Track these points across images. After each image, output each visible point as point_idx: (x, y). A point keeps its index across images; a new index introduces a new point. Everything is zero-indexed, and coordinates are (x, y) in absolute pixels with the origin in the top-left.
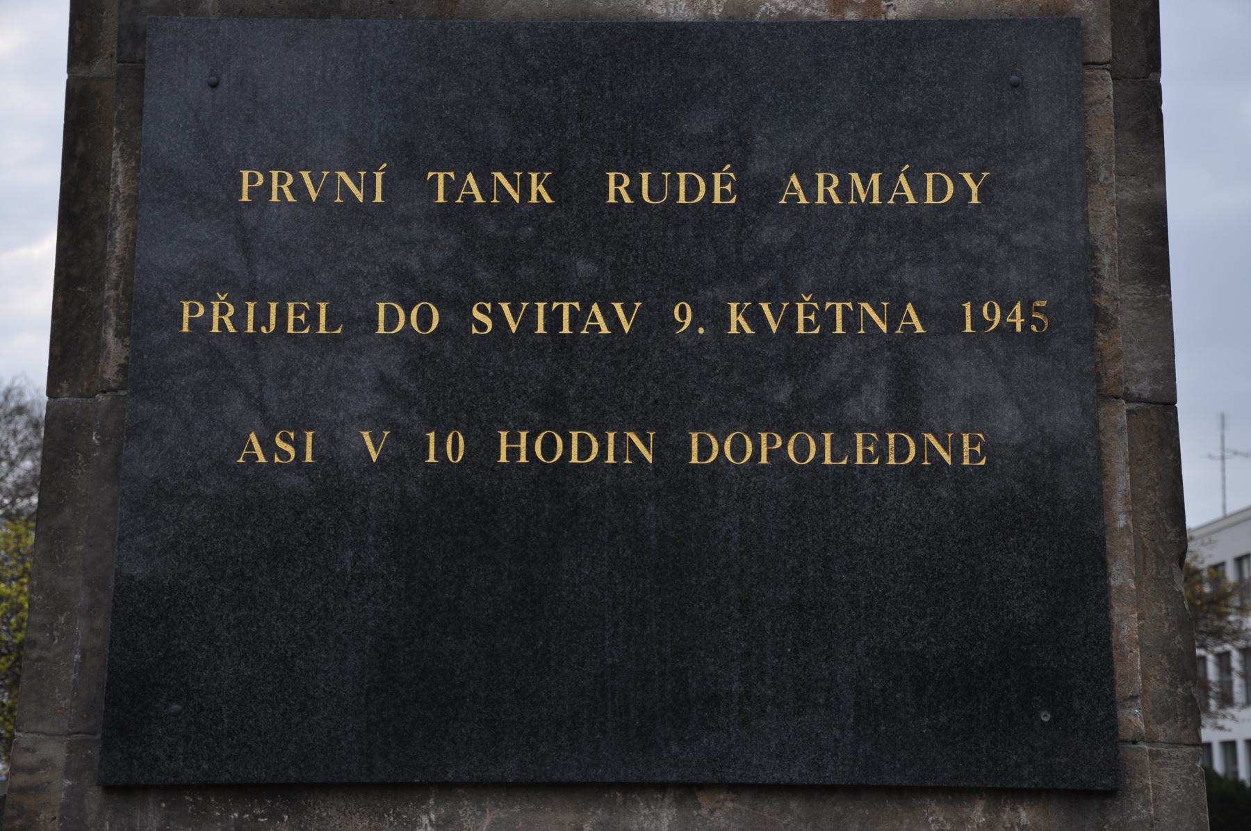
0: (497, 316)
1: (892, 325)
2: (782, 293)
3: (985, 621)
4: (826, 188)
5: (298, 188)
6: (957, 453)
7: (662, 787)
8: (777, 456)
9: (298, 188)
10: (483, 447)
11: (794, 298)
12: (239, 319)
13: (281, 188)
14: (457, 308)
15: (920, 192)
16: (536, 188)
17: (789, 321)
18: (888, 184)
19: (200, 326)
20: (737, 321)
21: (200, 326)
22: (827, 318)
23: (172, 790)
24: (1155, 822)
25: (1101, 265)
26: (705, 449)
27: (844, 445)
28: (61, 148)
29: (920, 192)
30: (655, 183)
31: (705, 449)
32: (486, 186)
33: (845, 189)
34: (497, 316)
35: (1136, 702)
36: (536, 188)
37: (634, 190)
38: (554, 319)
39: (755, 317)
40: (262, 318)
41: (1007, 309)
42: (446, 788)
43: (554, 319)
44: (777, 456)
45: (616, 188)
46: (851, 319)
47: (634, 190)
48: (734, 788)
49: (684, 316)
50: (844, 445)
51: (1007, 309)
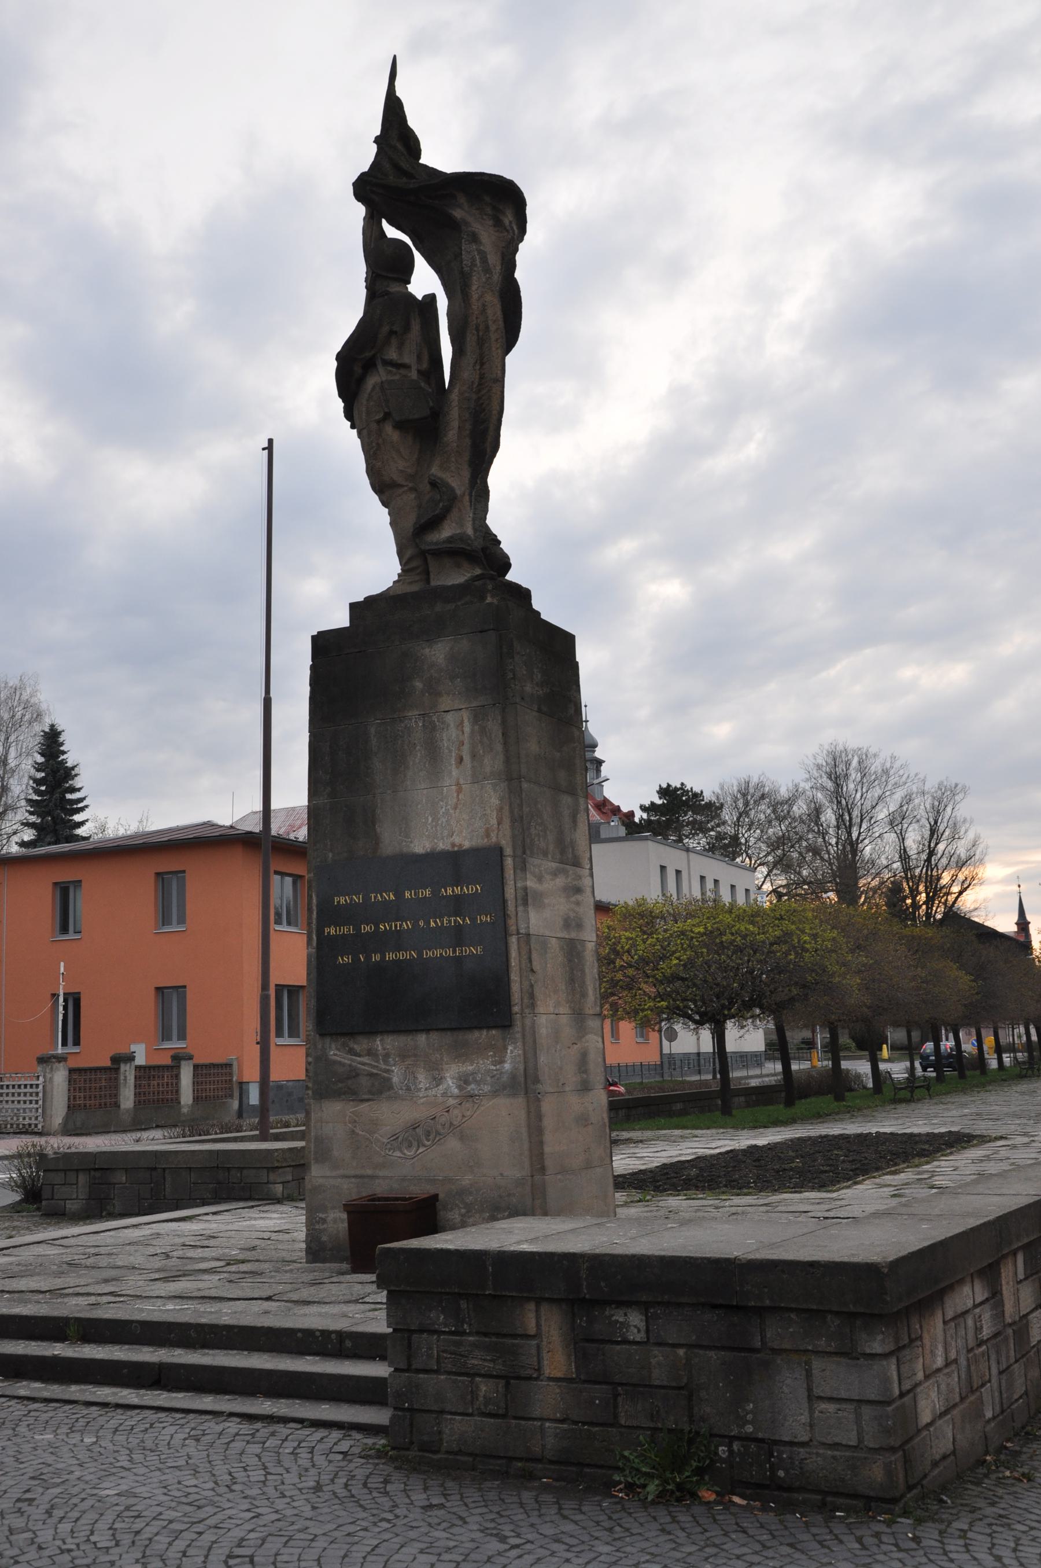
0: (385, 926)
1: (463, 922)
2: (441, 917)
4: (449, 891)
5: (346, 900)
6: (477, 951)
7: (423, 1030)
8: (441, 954)
9: (346, 900)
10: (383, 957)
11: (443, 918)
12: (336, 931)
13: (342, 901)
15: (468, 890)
16: (391, 896)
17: (442, 923)
18: (462, 889)
20: (433, 924)
21: (339, 902)
23: (331, 1035)
26: (427, 953)
29: (468, 890)
31: (427, 953)
32: (382, 896)
33: (453, 891)
34: (385, 926)
35: (777, 1050)
36: (391, 896)
38: (396, 926)
39: (436, 922)
40: (340, 931)
41: (486, 917)
42: (382, 1033)
43: (396, 926)
44: (441, 954)
45: (407, 895)
46: (455, 921)
48: (437, 1030)
49: (421, 923)
51: (486, 917)
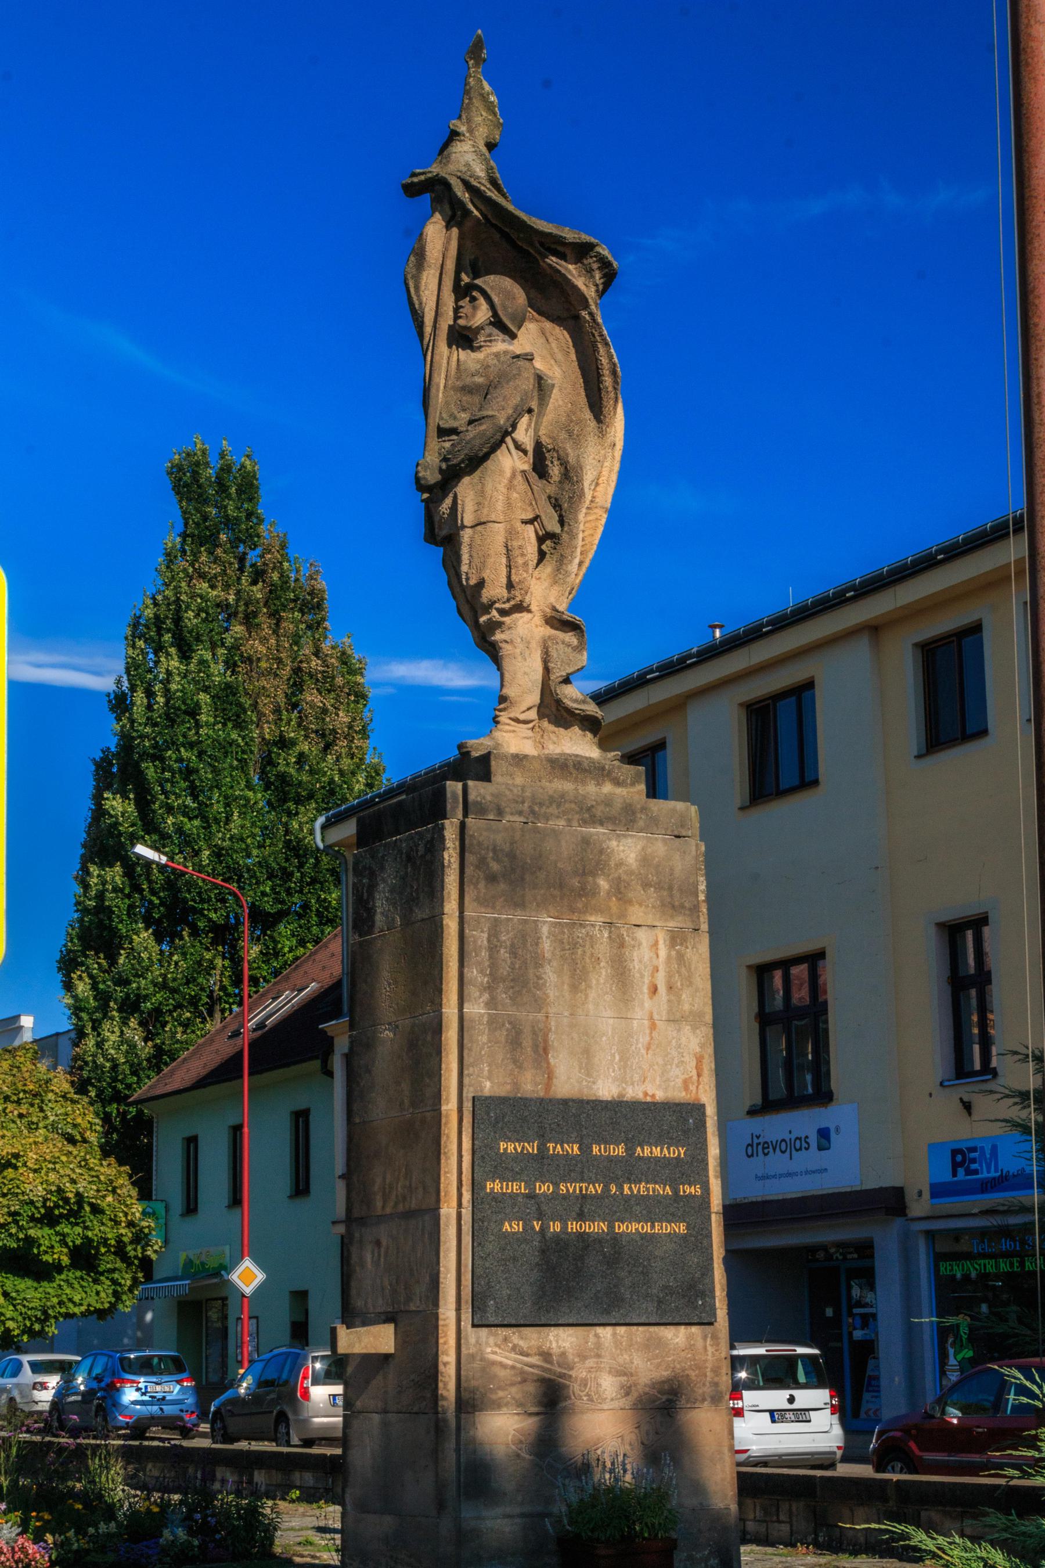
3: (249, 786)
5: (515, 1148)
9: (515, 1148)
10: (564, 1227)
12: (502, 1188)
14: (556, 1185)
19: (492, 1189)
21: (492, 1189)
22: (648, 1189)
24: (228, 875)
25: (458, 155)
26: (619, 1227)
27: (653, 1227)
28: (5, 820)
30: (605, 1148)
31: (619, 1227)
37: (600, 1150)
38: (581, 1189)
43: (581, 1189)
45: (595, 1150)
46: (654, 1190)
47: (600, 1150)
49: (613, 1189)
50: (653, 1227)
